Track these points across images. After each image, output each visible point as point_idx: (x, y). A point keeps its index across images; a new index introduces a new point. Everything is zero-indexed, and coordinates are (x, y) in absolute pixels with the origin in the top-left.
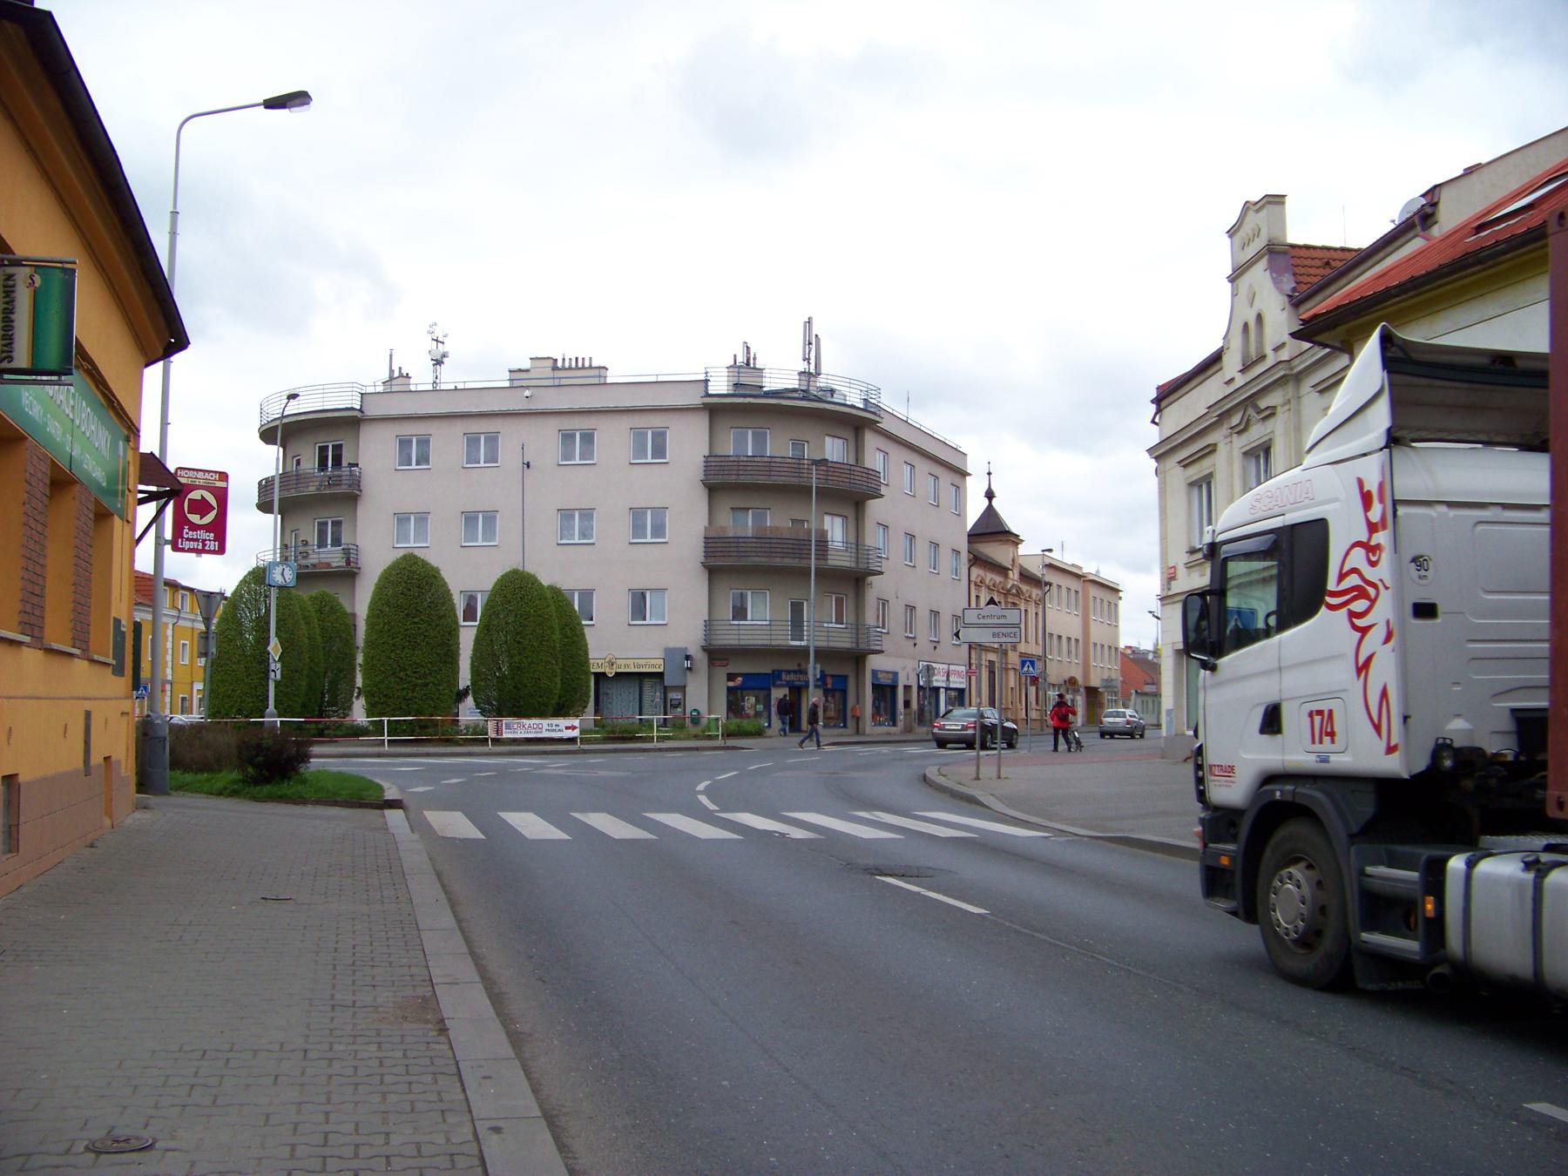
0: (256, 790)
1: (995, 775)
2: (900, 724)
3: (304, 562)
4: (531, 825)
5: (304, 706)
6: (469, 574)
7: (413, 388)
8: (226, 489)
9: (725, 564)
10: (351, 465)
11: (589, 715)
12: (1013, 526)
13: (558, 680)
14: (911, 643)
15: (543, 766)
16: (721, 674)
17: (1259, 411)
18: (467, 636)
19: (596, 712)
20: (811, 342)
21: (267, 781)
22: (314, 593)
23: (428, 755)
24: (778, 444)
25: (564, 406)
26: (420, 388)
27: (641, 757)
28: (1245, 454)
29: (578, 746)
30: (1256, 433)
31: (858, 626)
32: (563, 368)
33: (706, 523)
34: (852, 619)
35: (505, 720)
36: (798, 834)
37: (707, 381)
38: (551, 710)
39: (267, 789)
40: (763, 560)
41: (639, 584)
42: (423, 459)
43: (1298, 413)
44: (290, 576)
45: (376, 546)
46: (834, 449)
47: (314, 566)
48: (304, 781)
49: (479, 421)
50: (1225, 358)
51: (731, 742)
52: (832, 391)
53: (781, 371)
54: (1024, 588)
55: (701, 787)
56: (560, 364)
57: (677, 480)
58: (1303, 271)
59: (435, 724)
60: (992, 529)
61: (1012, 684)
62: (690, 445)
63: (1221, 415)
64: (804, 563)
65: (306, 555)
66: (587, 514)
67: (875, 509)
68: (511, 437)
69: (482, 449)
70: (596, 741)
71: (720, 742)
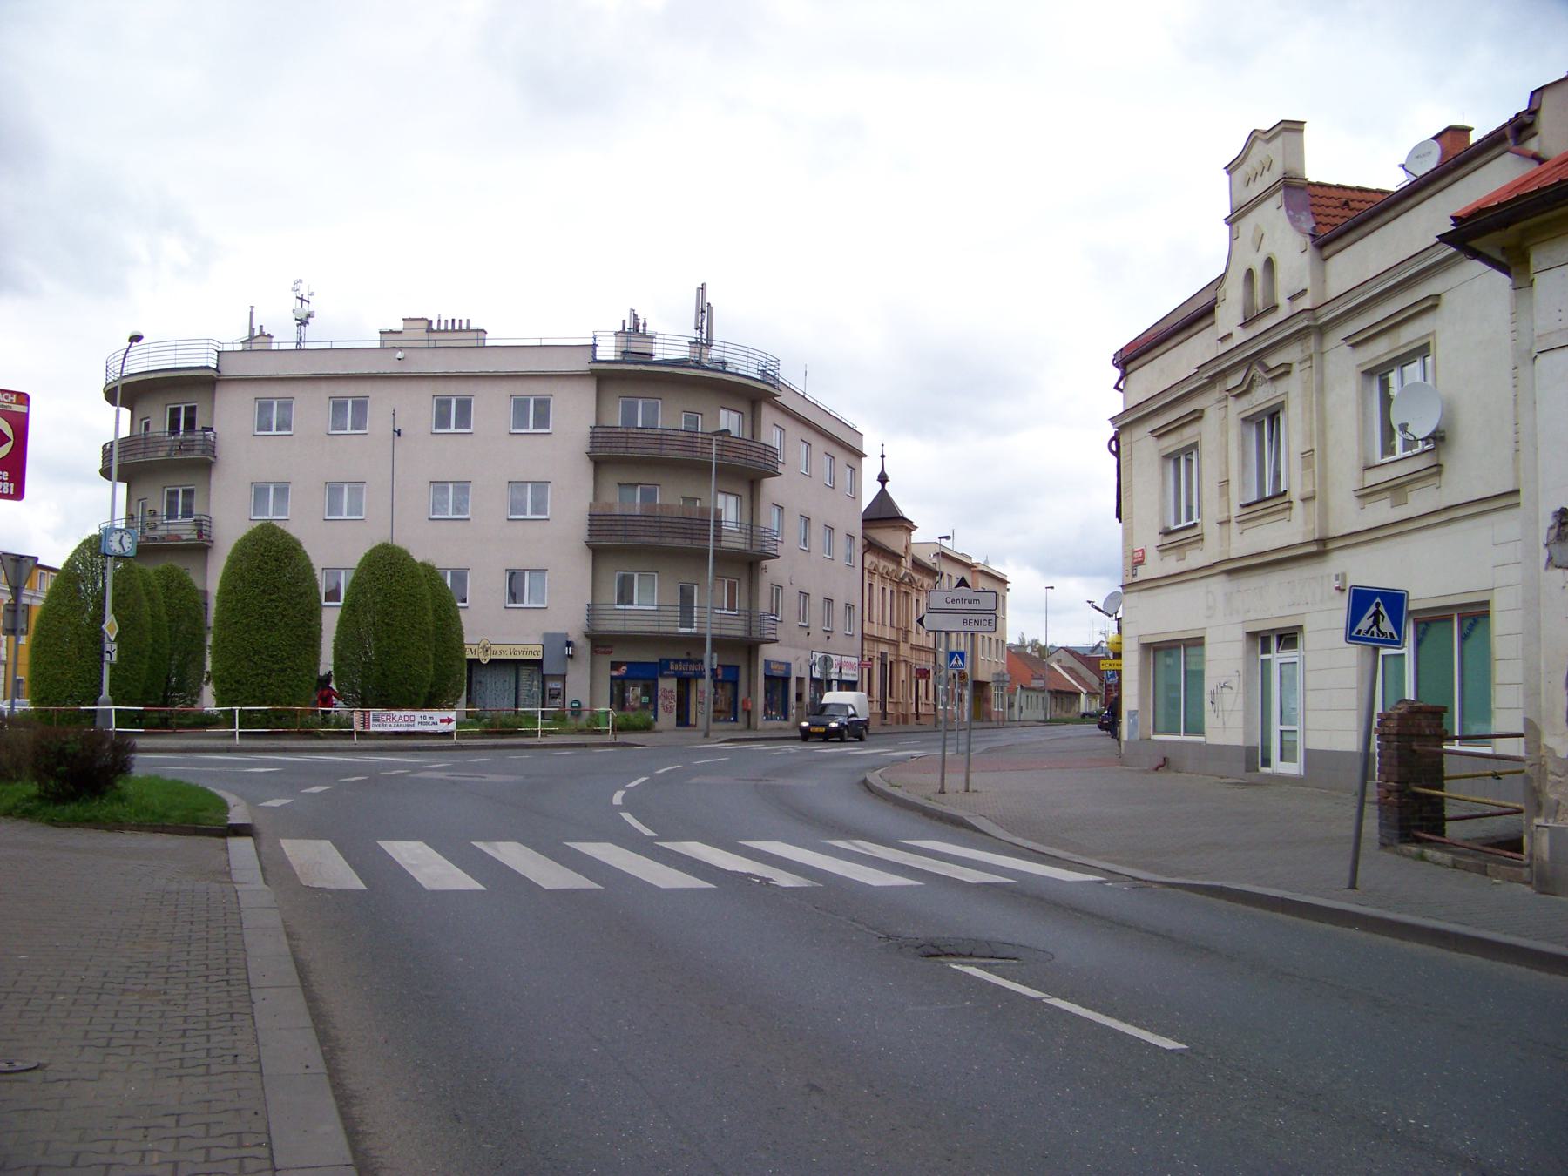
0: (53, 810)
1: (962, 787)
2: (792, 719)
3: (151, 534)
4: (425, 864)
5: (146, 692)
6: (334, 551)
7: (274, 347)
8: (27, 415)
9: (610, 543)
10: (205, 429)
11: (462, 707)
12: (906, 510)
13: (430, 667)
14: (805, 632)
15: (416, 768)
16: (604, 662)
17: (1268, 371)
18: (330, 618)
19: (469, 701)
20: (704, 311)
21: (73, 798)
22: (160, 567)
23: (285, 750)
24: (669, 415)
25: (439, 370)
26: (282, 347)
27: (526, 756)
28: (1244, 420)
29: (454, 741)
30: (1262, 396)
31: (751, 613)
32: (439, 331)
33: (591, 499)
34: (745, 605)
35: (373, 712)
36: (785, 880)
37: (595, 346)
38: (422, 699)
39: (71, 809)
40: (653, 541)
41: (515, 565)
42: (284, 424)
43: (1321, 371)
44: (128, 544)
45: (230, 517)
46: (729, 421)
47: (163, 538)
48: (122, 799)
49: (347, 385)
50: (1219, 312)
51: (621, 738)
52: (724, 363)
53: (671, 342)
54: (917, 577)
55: (618, 798)
56: (435, 326)
57: (561, 451)
58: (1320, 210)
59: (294, 714)
60: (884, 515)
61: (903, 677)
62: (575, 415)
63: (1213, 376)
64: (696, 544)
65: (154, 527)
66: (462, 487)
67: (771, 488)
68: (382, 402)
69: (350, 413)
70: (473, 735)
71: (609, 738)
